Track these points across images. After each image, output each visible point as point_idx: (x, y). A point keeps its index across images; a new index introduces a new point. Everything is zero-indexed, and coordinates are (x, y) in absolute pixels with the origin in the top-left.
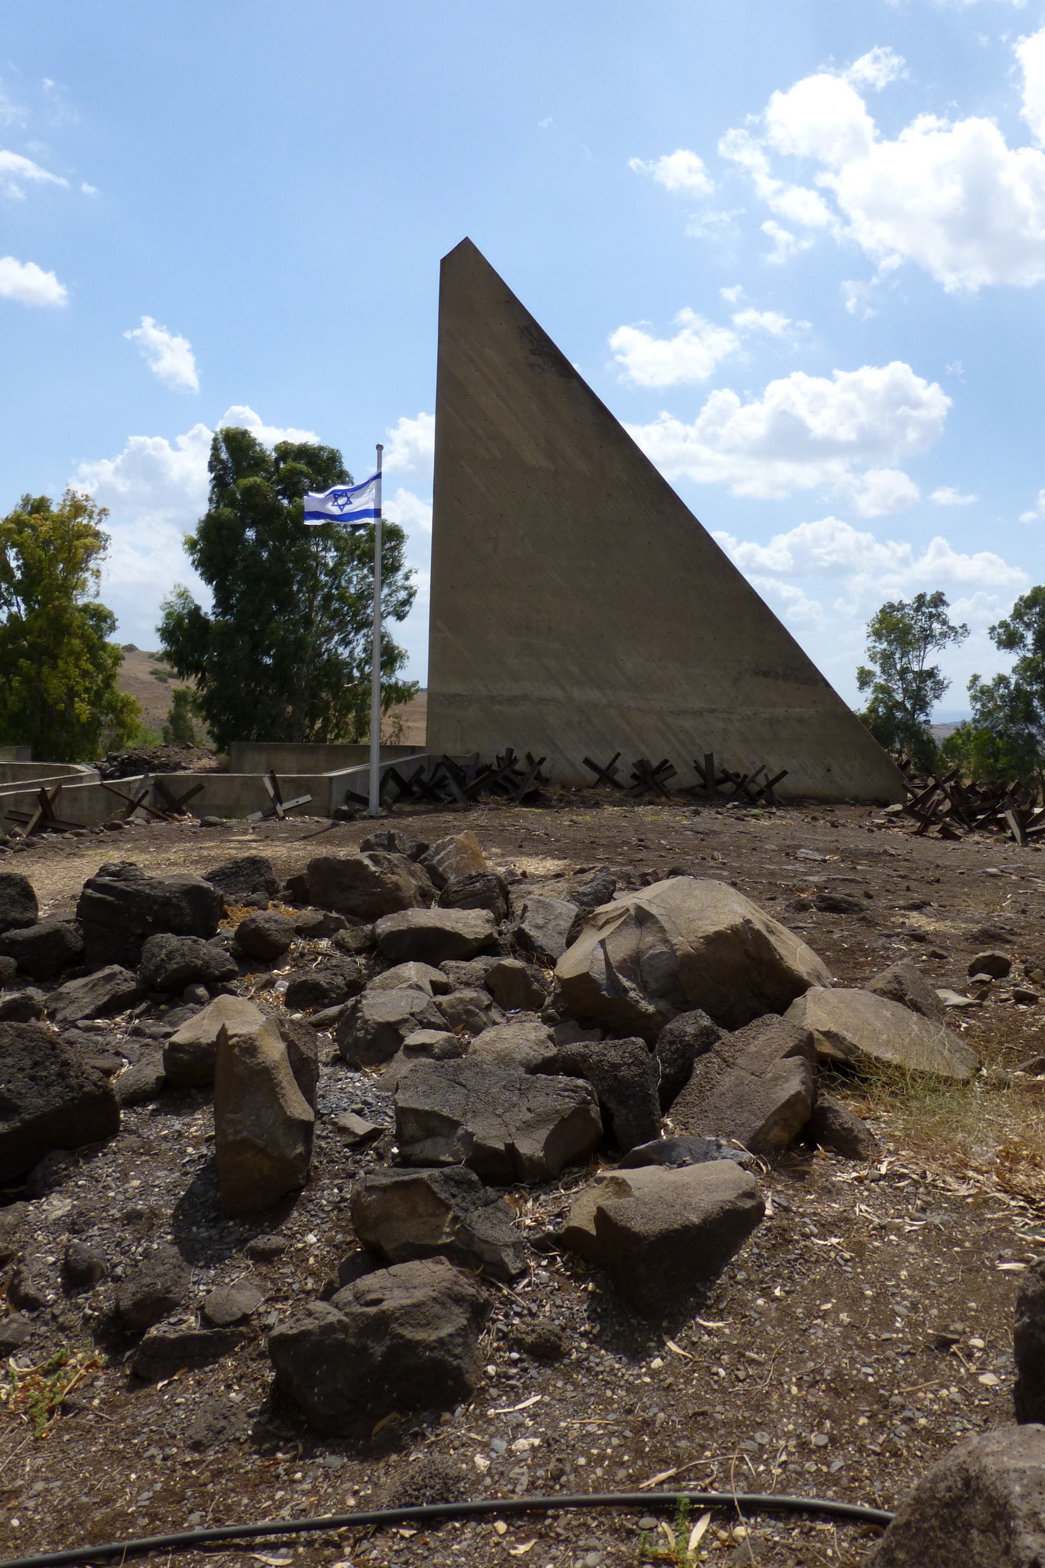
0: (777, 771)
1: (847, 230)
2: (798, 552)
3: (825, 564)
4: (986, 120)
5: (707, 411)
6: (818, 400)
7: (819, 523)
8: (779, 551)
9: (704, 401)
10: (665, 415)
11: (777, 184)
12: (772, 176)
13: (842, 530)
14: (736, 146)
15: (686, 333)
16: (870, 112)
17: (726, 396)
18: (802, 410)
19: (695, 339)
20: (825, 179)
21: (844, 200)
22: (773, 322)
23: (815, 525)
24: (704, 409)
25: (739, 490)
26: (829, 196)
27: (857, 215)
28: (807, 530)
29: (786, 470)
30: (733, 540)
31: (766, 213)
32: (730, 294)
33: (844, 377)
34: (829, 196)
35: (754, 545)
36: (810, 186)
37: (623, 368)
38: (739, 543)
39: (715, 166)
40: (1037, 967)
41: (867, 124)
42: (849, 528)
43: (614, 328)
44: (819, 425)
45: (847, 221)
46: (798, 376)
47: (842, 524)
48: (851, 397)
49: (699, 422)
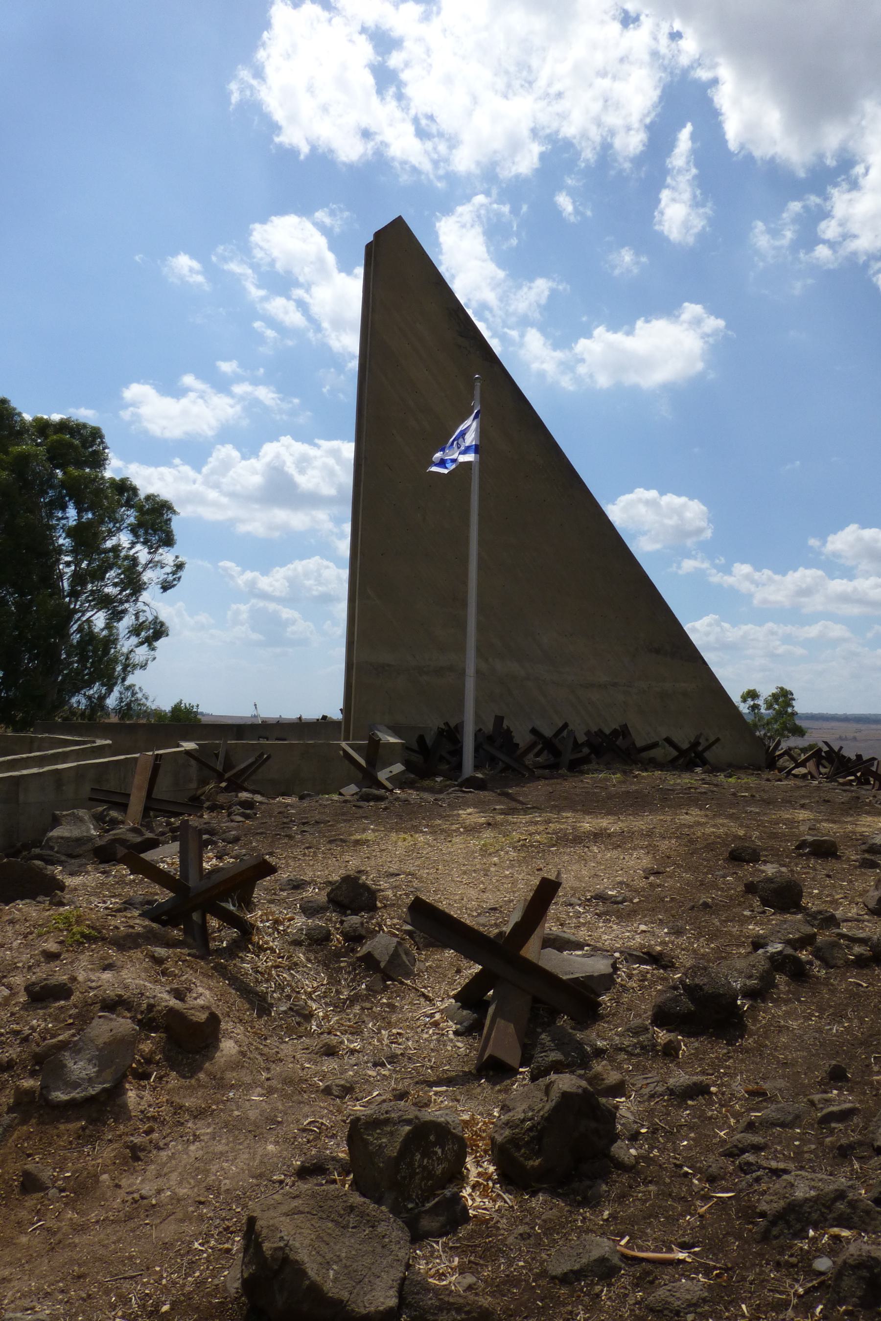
0: (712, 739)
1: (319, 336)
2: (292, 582)
3: (315, 593)
4: (166, 706)
5: (213, 462)
6: (303, 463)
7: (308, 561)
8: (277, 581)
9: (210, 455)
10: (177, 461)
11: (262, 293)
12: (258, 287)
13: (327, 567)
14: (225, 260)
15: (192, 395)
16: (332, 248)
17: (227, 451)
18: (290, 468)
19: (200, 401)
20: (299, 293)
21: (315, 310)
22: (265, 394)
23: (305, 562)
24: (210, 459)
25: (242, 528)
26: (302, 306)
27: (325, 325)
28: (299, 566)
29: (281, 515)
30: (239, 569)
31: (255, 315)
32: (227, 367)
33: (326, 444)
34: (302, 306)
35: (257, 574)
36: (289, 298)
37: (137, 418)
38: (243, 572)
39: (211, 271)
40: (588, 945)
41: (330, 258)
42: (331, 564)
43: (127, 384)
44: (306, 481)
45: (318, 328)
46: (287, 440)
47: (325, 563)
48: (331, 461)
49: (205, 470)
